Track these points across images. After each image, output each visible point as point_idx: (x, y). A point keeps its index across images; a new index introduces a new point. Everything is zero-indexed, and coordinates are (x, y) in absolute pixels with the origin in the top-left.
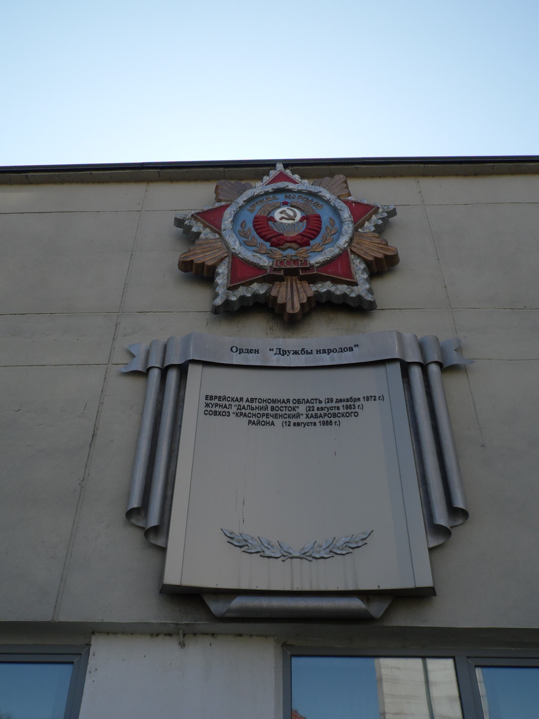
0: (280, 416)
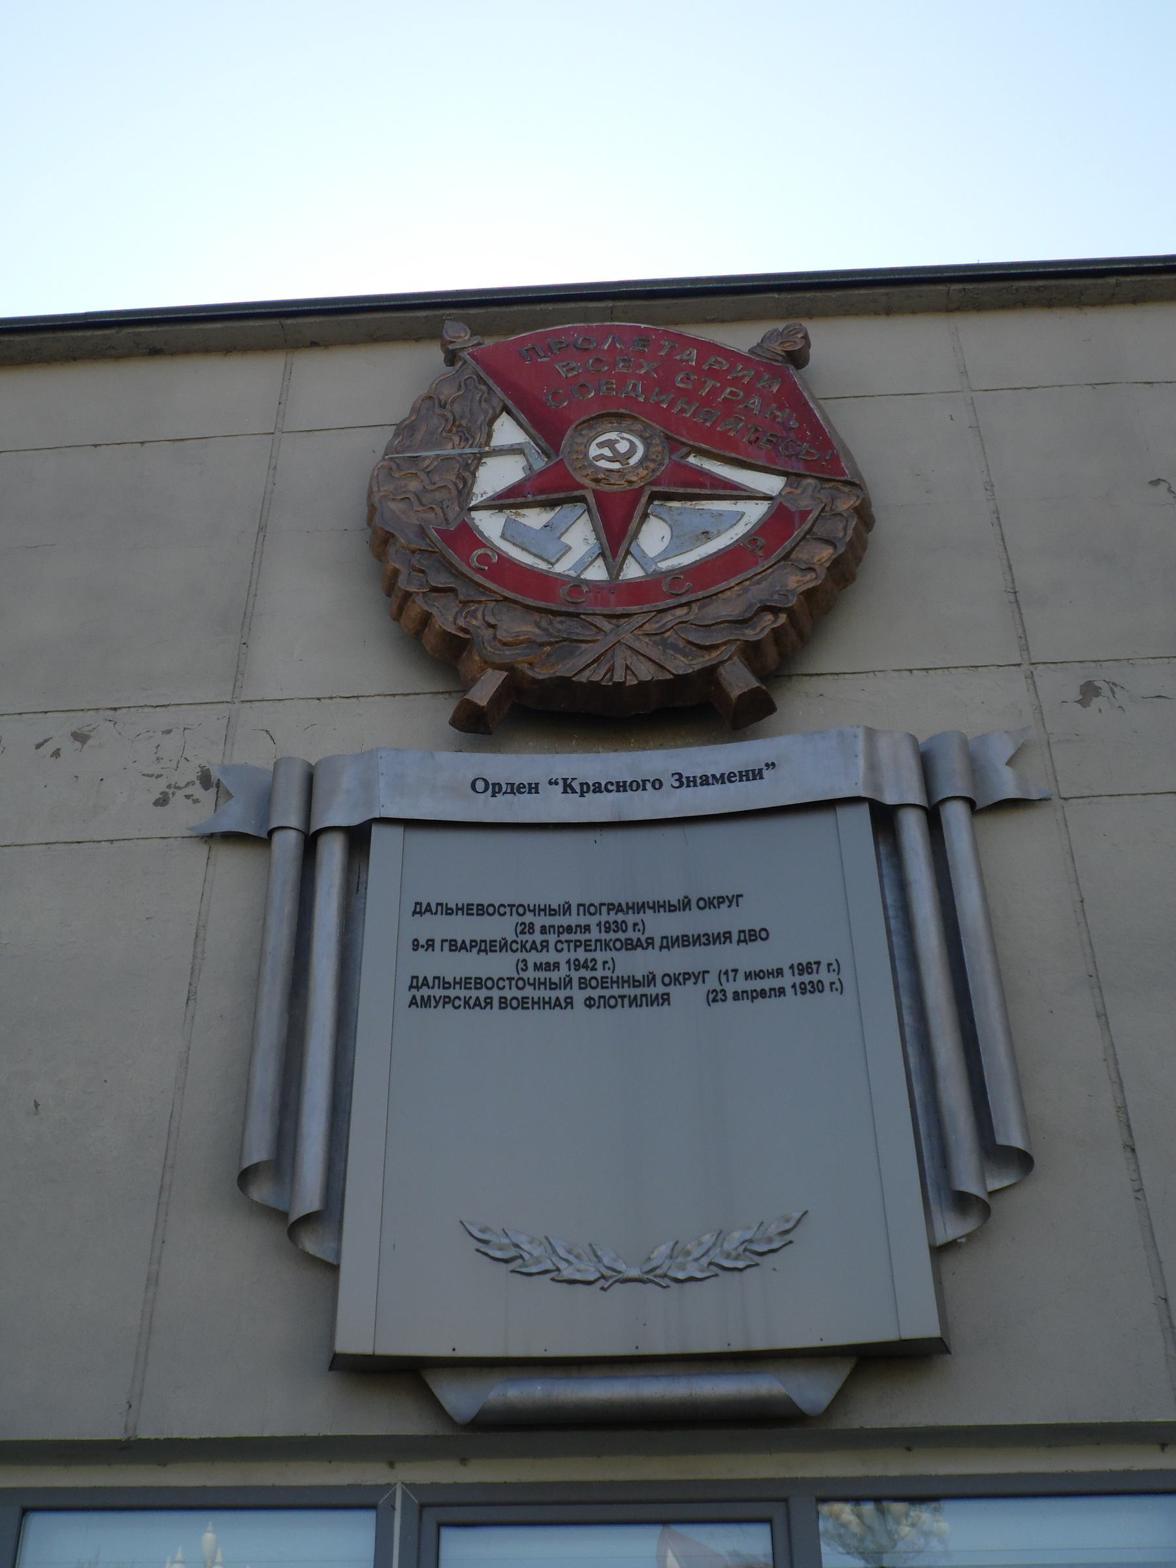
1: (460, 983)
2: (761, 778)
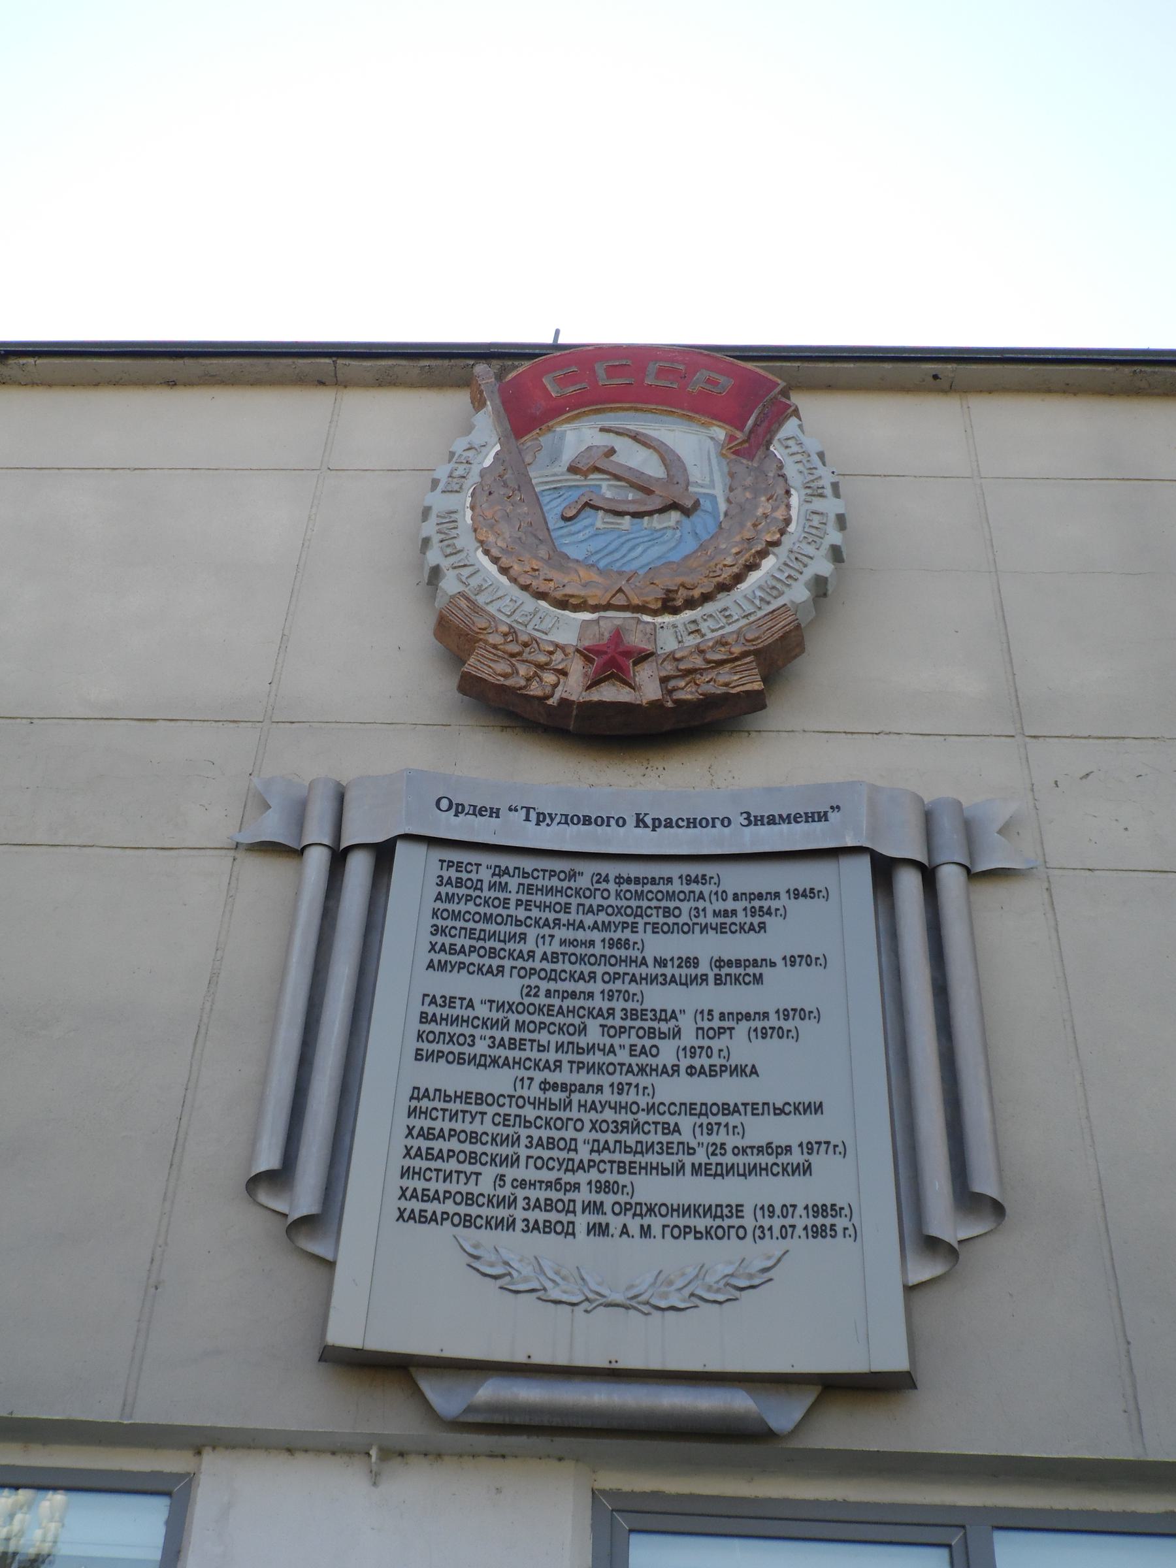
0: (538, 890)
1: (461, 1097)
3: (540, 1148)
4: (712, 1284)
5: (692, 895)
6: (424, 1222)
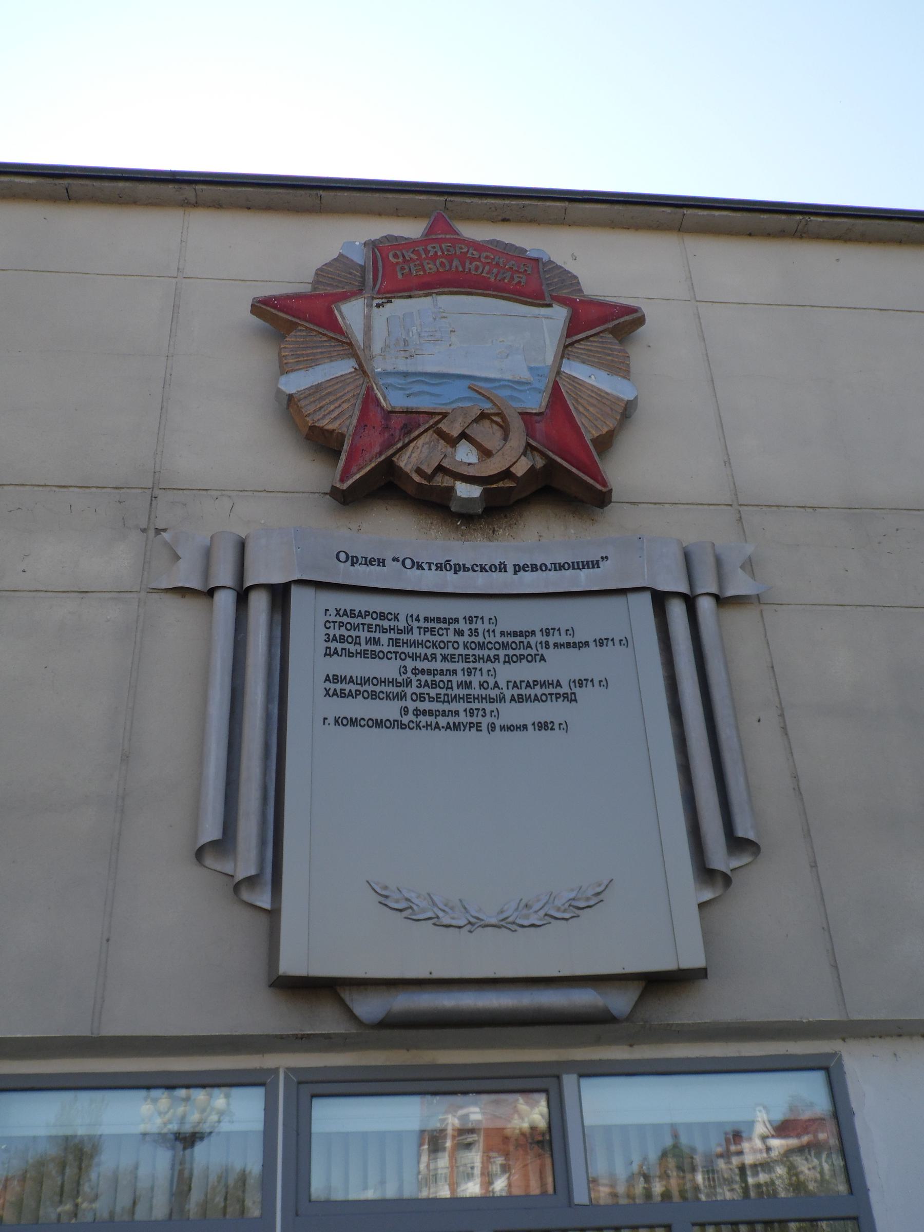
2: (598, 567)
3: (426, 688)
4: (560, 905)
5: (522, 644)
6: (344, 697)
